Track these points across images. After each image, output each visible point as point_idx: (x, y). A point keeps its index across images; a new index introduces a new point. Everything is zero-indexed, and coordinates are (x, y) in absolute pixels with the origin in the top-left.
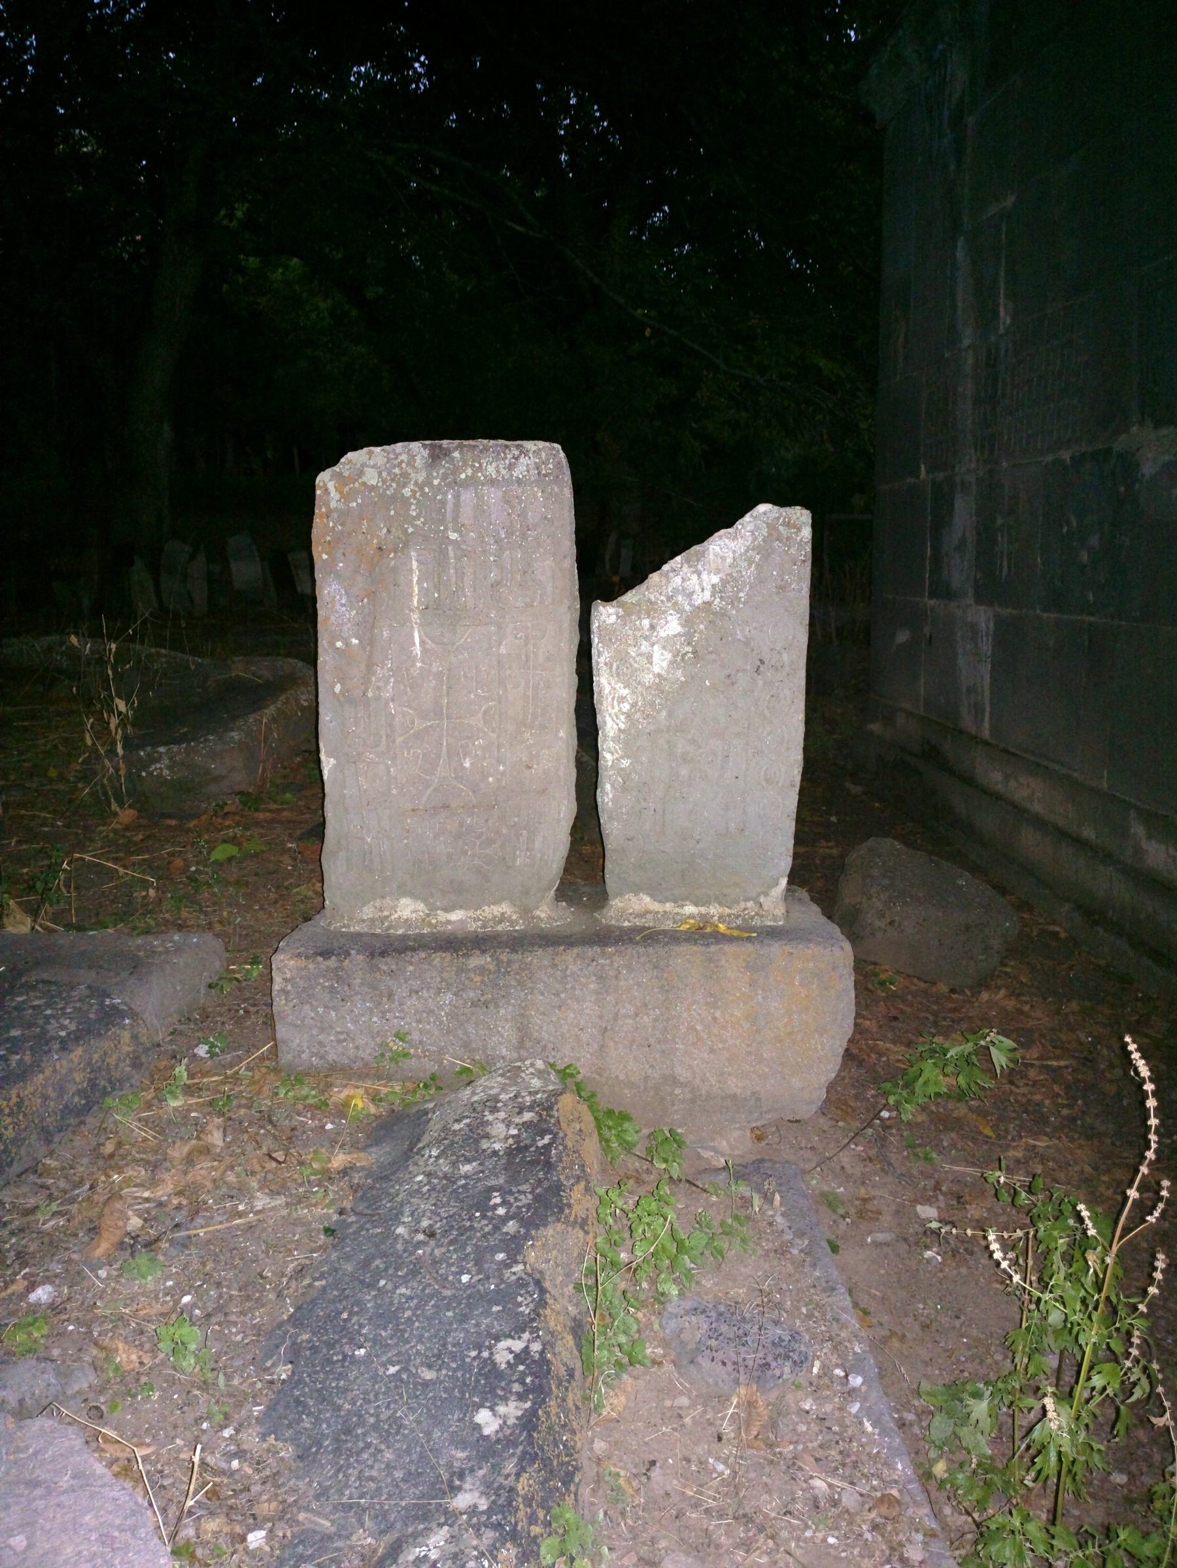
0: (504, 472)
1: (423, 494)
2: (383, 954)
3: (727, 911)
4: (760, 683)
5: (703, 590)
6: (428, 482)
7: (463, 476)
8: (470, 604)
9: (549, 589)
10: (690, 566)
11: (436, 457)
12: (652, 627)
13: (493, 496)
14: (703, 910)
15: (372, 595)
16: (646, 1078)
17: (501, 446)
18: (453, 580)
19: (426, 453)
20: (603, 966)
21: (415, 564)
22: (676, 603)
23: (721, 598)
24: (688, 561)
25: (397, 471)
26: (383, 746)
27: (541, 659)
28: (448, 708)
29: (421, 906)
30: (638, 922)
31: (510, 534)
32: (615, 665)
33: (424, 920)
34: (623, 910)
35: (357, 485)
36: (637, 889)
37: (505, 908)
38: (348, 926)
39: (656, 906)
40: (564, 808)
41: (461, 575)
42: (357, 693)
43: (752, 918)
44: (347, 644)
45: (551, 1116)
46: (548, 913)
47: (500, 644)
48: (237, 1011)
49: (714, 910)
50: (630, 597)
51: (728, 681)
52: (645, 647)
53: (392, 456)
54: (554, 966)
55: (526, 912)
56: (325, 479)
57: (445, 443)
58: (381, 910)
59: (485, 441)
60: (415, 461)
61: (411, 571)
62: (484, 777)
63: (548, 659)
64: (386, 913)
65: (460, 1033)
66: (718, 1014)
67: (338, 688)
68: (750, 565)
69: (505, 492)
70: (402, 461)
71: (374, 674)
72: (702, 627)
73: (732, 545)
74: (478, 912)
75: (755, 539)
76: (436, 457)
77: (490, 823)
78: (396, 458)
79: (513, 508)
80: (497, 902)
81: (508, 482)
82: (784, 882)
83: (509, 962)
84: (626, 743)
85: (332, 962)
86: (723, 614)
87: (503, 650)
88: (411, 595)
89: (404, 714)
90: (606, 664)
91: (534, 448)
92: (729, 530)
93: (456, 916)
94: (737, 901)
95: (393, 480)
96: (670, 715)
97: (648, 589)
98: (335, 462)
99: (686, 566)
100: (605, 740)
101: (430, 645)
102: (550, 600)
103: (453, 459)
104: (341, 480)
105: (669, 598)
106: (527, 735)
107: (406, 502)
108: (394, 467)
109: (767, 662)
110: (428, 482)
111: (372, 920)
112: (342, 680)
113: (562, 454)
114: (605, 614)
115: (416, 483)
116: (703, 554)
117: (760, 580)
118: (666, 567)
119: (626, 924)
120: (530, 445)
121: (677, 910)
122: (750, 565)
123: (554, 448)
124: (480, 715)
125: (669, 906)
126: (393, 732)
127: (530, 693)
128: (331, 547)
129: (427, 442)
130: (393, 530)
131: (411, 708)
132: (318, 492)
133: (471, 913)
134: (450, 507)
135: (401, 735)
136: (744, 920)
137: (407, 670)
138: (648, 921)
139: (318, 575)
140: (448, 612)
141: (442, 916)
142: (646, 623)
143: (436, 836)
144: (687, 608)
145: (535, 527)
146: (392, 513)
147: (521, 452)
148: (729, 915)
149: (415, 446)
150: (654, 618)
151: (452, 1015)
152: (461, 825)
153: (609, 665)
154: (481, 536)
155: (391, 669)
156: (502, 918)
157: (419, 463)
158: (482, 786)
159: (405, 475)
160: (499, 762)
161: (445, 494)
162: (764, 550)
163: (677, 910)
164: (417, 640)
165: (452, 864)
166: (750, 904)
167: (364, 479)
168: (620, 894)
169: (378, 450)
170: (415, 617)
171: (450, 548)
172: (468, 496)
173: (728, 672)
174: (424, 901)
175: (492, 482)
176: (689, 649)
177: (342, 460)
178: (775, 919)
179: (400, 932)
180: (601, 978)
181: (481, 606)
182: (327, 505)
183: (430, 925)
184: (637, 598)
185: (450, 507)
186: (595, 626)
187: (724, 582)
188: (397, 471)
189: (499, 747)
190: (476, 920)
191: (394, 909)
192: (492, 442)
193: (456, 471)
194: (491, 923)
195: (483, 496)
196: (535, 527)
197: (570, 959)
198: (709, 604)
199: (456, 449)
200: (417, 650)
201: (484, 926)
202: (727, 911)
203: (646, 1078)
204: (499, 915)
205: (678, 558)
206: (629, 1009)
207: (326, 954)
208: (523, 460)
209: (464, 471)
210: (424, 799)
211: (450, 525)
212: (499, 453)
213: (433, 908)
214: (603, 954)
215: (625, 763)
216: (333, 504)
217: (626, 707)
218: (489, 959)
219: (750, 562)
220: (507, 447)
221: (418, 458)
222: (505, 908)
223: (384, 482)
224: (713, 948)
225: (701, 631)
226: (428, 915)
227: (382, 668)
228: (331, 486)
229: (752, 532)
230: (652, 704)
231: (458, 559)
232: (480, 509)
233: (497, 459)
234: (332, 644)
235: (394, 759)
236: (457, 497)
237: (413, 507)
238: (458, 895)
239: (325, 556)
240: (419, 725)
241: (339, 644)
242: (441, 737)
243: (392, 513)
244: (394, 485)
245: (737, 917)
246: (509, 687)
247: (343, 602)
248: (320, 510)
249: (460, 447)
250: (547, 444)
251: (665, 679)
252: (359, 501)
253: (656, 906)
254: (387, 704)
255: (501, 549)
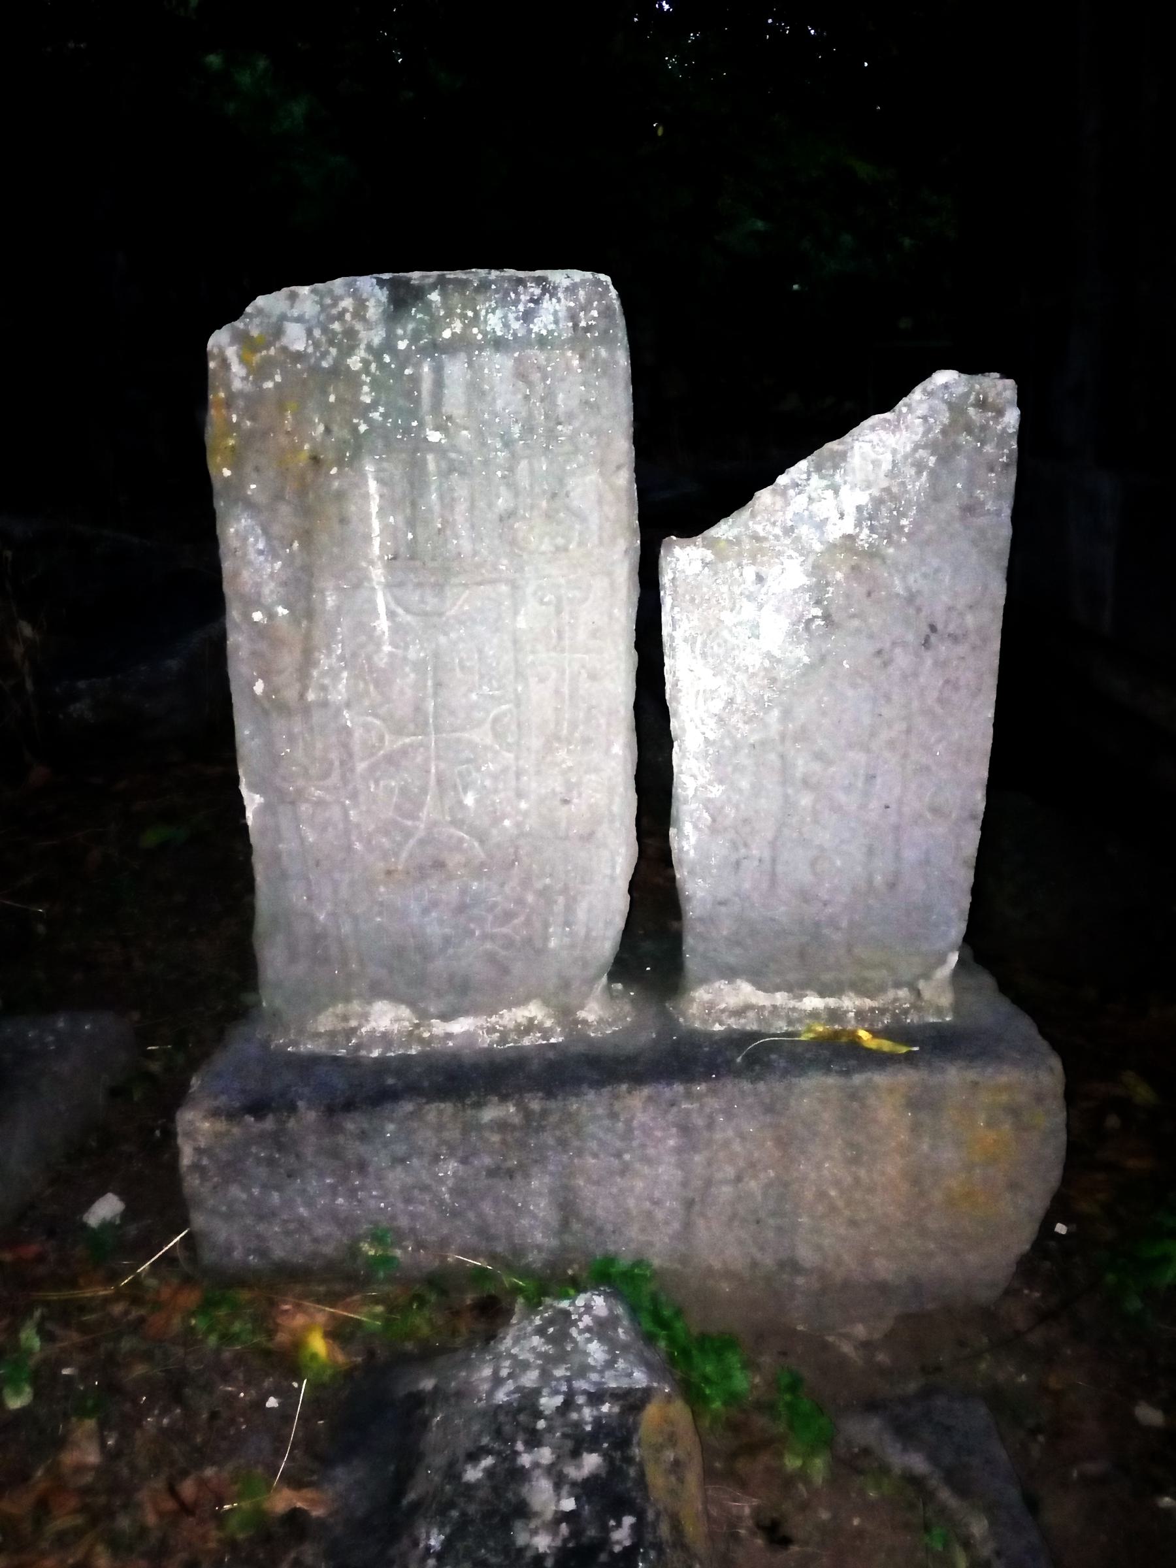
0: (515, 325)
1: (382, 366)
2: (349, 1106)
3: (868, 1003)
4: (929, 662)
5: (842, 516)
6: (389, 345)
7: (447, 334)
8: (466, 546)
9: (594, 520)
10: (822, 477)
11: (403, 300)
12: (760, 579)
13: (498, 367)
14: (832, 1002)
15: (307, 537)
16: (754, 1265)
17: (510, 279)
18: (437, 508)
19: (383, 295)
20: (688, 1113)
21: (373, 486)
22: (798, 538)
23: (872, 529)
24: (819, 468)
25: (336, 326)
26: (335, 778)
27: (582, 635)
28: (436, 717)
29: (405, 1012)
30: (734, 1023)
31: (529, 429)
32: (700, 640)
33: (411, 1033)
34: (711, 1005)
35: (272, 351)
36: (731, 973)
37: (534, 1011)
38: (295, 1043)
39: (760, 998)
40: (617, 855)
41: (448, 502)
42: (290, 695)
43: (906, 1012)
44: (271, 615)
45: (629, 1460)
46: (601, 1014)
47: (516, 613)
48: (152, 1131)
49: (849, 1003)
50: (723, 530)
51: (878, 662)
52: (748, 610)
53: (328, 301)
54: (613, 1116)
55: (565, 1014)
56: (220, 340)
57: (415, 276)
58: (345, 1018)
59: (483, 272)
60: (365, 308)
61: (366, 496)
62: (497, 821)
63: (594, 634)
64: (353, 1023)
65: (471, 1215)
66: (862, 1173)
67: (259, 687)
68: (919, 473)
69: (519, 361)
70: (345, 310)
71: (316, 664)
72: (839, 576)
73: (891, 440)
74: (494, 1019)
75: (928, 430)
76: (403, 300)
77: (507, 889)
78: (335, 305)
79: (530, 384)
80: (523, 1002)
81: (523, 342)
82: (954, 958)
83: (544, 1113)
84: (717, 762)
85: (269, 1124)
86: (873, 554)
87: (522, 623)
88: (367, 538)
89: (367, 727)
90: (686, 640)
91: (566, 283)
92: (888, 415)
93: (460, 1026)
94: (881, 989)
95: (331, 343)
96: (787, 714)
97: (753, 515)
98: (235, 313)
99: (815, 477)
100: (683, 757)
101: (404, 617)
102: (595, 539)
103: (428, 304)
104: (246, 342)
105: (789, 531)
106: (562, 754)
107: (353, 380)
108: (332, 319)
109: (940, 627)
110: (389, 345)
111: (332, 1034)
112: (265, 675)
113: (613, 293)
114: (682, 559)
115: (369, 348)
116: (843, 456)
117: (936, 495)
118: (782, 480)
119: (717, 1027)
120: (559, 277)
121: (792, 1003)
122: (919, 473)
123: (599, 283)
124: (487, 726)
125: (780, 998)
126: (350, 755)
127: (566, 690)
128: (237, 459)
129: (386, 276)
130: (335, 428)
131: (376, 715)
132: (212, 365)
133: (481, 1021)
134: (426, 386)
135: (362, 759)
136: (894, 1015)
137: (369, 659)
138: (750, 1024)
139: (220, 504)
140: (430, 564)
141: (439, 1027)
142: (750, 572)
143: (426, 911)
144: (818, 547)
145: (570, 417)
146: (332, 399)
147: (545, 290)
148: (872, 1010)
149: (366, 283)
150: (762, 564)
151: (458, 1191)
152: (464, 891)
153: (691, 641)
154: (480, 435)
155: (341, 658)
156: (531, 1026)
157: (373, 312)
158: (494, 832)
159: (350, 333)
160: (520, 795)
161: (418, 366)
162: (944, 449)
163: (792, 1003)
164: (382, 609)
165: (451, 951)
166: (903, 993)
167: (285, 341)
168: (704, 980)
169: (305, 290)
170: (377, 574)
171: (430, 457)
172: (456, 369)
173: (878, 646)
174: (412, 1004)
175: (498, 344)
176: (818, 612)
177: (249, 309)
178: (939, 1011)
179: (375, 1054)
180: (685, 1129)
181: (484, 552)
182: (227, 386)
183: (421, 1040)
184: (735, 531)
185: (426, 386)
186: (666, 579)
187: (878, 502)
188: (336, 326)
189: (518, 775)
190: (491, 1030)
191: (365, 1017)
192: (494, 274)
193: (435, 325)
194: (514, 1036)
195: (482, 368)
196: (570, 417)
197: (638, 1105)
198: (851, 538)
199: (433, 287)
200: (383, 624)
201: (503, 1039)
202: (868, 1003)
203: (754, 1265)
204: (525, 1022)
205: (803, 464)
206: (730, 1171)
207: (258, 1108)
208: (548, 305)
209: (449, 325)
210: (404, 855)
211: (429, 418)
212: (507, 294)
213: (424, 1016)
214: (689, 1096)
215: (716, 791)
216: (237, 385)
217: (717, 706)
218: (512, 1109)
219: (920, 466)
220: (520, 282)
221: (371, 304)
222: (534, 1011)
223: (317, 345)
224: (858, 1079)
225: (838, 583)
226: (417, 1026)
227: (329, 655)
228: (231, 352)
229: (925, 418)
230: (759, 701)
231: (445, 474)
232: (476, 390)
233: (504, 302)
234: (247, 616)
235: (354, 796)
236: (438, 370)
237: (366, 389)
238: (463, 995)
239: (227, 473)
240: (392, 743)
241: (257, 616)
242: (427, 760)
243: (332, 399)
244: (334, 351)
245: (883, 1011)
246: (533, 681)
247: (261, 546)
248: (217, 395)
249: (441, 284)
250: (588, 275)
251: (779, 661)
252: (278, 378)
253: (760, 998)
254: (338, 713)
255: (514, 458)
